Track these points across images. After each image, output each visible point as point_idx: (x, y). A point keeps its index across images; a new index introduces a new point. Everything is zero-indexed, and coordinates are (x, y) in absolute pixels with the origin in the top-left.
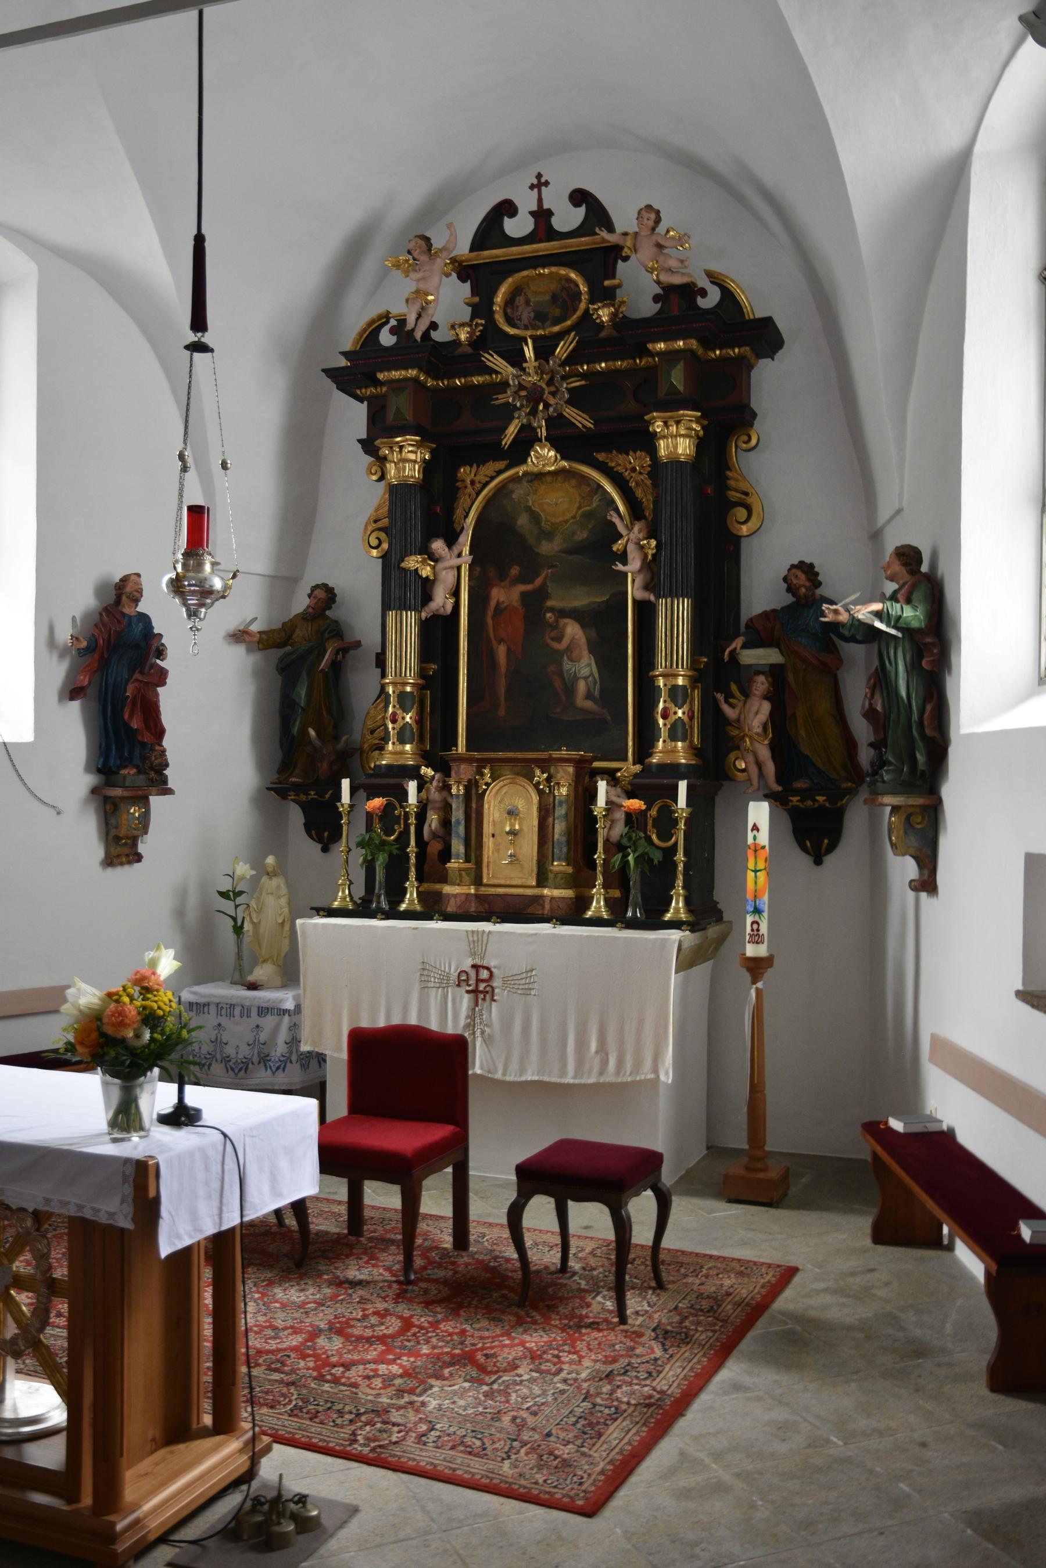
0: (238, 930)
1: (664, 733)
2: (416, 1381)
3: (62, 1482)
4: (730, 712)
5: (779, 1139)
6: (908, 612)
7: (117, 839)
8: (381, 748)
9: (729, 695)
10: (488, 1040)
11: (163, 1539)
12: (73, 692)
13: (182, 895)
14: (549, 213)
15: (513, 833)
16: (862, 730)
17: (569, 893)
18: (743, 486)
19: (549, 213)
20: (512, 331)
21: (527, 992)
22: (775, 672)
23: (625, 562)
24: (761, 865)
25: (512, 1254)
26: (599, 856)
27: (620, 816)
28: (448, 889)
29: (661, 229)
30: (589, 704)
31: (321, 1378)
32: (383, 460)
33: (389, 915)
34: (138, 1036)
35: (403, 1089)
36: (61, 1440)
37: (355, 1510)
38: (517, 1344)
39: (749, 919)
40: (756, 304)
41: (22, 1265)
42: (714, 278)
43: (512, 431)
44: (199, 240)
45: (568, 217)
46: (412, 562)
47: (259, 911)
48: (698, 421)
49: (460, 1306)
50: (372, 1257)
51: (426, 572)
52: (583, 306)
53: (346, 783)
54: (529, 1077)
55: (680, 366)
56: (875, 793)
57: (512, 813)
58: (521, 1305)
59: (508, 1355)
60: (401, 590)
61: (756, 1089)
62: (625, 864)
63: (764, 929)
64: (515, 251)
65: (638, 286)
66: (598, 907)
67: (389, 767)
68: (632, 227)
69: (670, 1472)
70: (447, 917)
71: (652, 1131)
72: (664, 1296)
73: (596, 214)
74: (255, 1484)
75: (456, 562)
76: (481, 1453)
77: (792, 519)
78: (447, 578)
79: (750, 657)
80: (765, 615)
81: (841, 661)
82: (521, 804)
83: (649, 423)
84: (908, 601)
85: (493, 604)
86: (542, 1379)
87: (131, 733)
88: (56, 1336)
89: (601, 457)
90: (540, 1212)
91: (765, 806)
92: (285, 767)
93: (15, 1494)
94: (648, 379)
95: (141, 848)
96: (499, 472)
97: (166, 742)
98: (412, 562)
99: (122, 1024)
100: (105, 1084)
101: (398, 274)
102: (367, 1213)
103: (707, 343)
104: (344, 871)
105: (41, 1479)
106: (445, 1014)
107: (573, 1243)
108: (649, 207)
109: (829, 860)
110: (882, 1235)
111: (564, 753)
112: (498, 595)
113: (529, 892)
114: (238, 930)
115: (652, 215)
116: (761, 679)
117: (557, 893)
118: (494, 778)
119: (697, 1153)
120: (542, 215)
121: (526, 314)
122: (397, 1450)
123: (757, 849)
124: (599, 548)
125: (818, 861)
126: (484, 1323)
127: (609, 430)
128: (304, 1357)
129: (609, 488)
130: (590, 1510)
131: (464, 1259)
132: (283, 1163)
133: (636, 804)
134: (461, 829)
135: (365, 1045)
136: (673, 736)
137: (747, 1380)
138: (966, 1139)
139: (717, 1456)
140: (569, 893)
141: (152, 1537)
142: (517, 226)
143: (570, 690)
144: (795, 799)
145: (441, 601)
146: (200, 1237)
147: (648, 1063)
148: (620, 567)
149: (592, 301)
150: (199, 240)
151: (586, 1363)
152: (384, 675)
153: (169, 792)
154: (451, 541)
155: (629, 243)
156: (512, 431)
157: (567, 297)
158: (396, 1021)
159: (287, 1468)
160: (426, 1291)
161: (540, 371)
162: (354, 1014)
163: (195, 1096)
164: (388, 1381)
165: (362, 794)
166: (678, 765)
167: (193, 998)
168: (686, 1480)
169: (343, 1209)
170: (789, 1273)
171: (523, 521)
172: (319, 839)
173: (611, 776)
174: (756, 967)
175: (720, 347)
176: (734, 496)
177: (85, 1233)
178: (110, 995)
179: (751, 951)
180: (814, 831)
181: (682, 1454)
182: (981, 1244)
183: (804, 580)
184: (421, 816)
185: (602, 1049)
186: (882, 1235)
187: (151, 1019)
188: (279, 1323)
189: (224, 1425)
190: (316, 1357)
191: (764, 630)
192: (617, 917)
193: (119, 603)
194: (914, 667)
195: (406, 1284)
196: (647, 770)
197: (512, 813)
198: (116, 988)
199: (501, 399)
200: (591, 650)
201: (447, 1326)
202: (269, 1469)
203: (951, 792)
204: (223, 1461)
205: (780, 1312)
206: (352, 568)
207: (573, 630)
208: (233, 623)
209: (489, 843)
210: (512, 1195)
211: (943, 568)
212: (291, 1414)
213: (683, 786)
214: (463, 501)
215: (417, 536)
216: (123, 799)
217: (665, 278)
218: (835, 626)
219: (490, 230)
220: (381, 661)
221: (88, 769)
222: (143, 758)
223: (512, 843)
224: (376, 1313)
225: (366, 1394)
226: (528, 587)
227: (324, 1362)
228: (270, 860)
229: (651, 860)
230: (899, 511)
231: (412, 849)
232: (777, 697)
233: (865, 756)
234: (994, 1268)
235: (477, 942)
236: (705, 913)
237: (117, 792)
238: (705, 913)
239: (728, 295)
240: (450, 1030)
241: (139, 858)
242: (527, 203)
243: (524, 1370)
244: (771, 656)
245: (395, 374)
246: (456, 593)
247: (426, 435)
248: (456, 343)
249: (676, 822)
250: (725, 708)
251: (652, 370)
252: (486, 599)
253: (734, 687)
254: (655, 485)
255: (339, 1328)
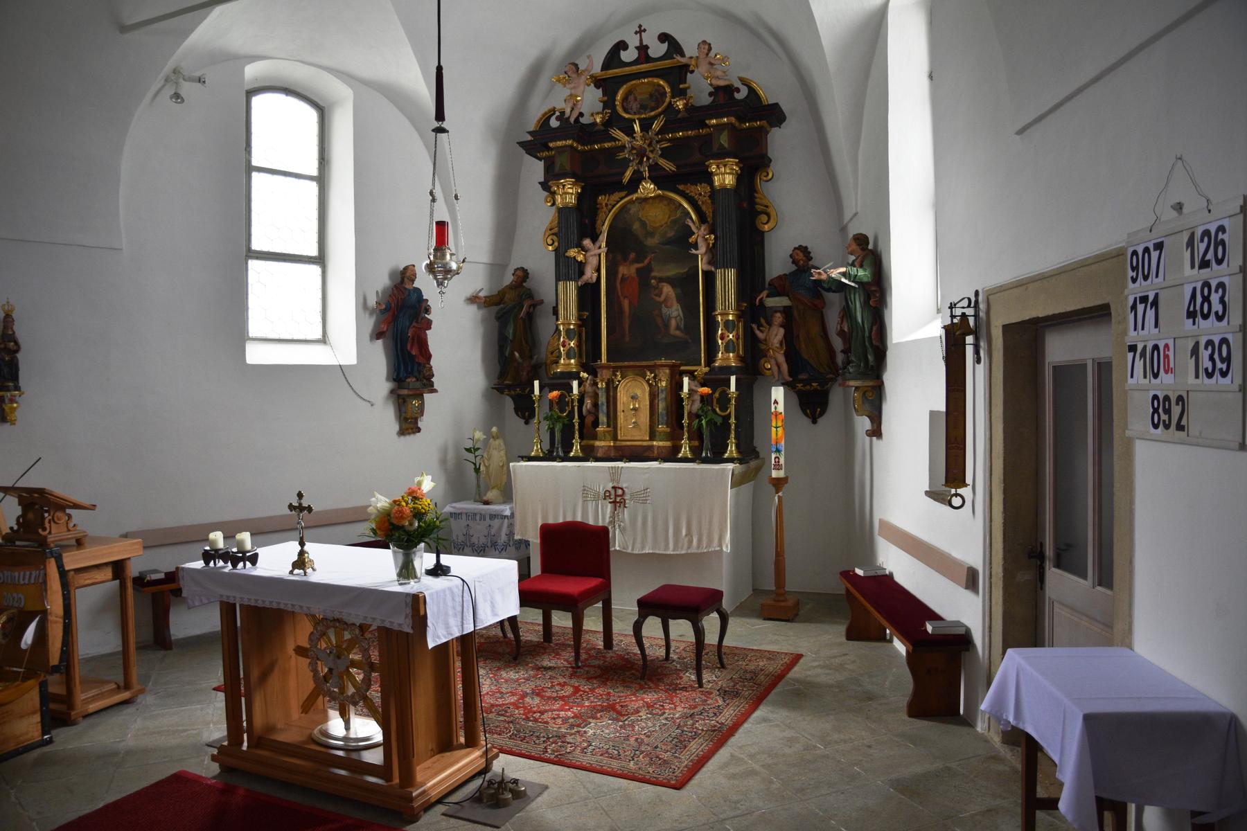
0: (477, 470)
1: (722, 348)
2: (582, 720)
3: (383, 771)
4: (761, 335)
5: (793, 584)
6: (861, 273)
7: (406, 419)
8: (557, 362)
9: (759, 326)
10: (623, 530)
11: (439, 801)
12: (378, 335)
13: (444, 451)
14: (647, 47)
15: (635, 409)
16: (838, 343)
17: (668, 444)
18: (765, 202)
19: (647, 47)
20: (626, 116)
21: (644, 502)
22: (786, 311)
23: (697, 249)
24: (780, 424)
25: (637, 650)
26: (685, 421)
27: (697, 398)
28: (597, 443)
29: (712, 54)
30: (678, 333)
31: (527, 719)
32: (553, 194)
33: (563, 460)
34: (411, 524)
35: (570, 560)
36: (381, 750)
37: (547, 787)
38: (638, 700)
39: (773, 456)
40: (768, 97)
41: (355, 656)
42: (744, 82)
43: (628, 174)
44: (439, 70)
45: (657, 49)
46: (572, 253)
47: (489, 459)
48: (737, 164)
49: (608, 679)
50: (558, 654)
51: (580, 258)
52: (668, 100)
53: (536, 383)
54: (647, 551)
55: (725, 133)
56: (845, 380)
57: (634, 398)
58: (642, 678)
59: (633, 706)
60: (567, 269)
61: (779, 555)
62: (700, 425)
63: (782, 461)
64: (627, 70)
65: (700, 87)
66: (685, 451)
67: (562, 373)
68: (695, 53)
69: (724, 766)
70: (597, 460)
71: (720, 579)
72: (725, 672)
73: (674, 46)
74: (488, 776)
75: (598, 251)
76: (618, 757)
77: (794, 220)
78: (593, 261)
79: (771, 302)
80: (780, 277)
81: (824, 303)
82: (639, 393)
83: (708, 166)
84: (861, 266)
85: (620, 276)
86: (652, 718)
87: (412, 357)
88: (375, 693)
89: (681, 187)
90: (653, 627)
91: (781, 389)
92: (502, 375)
93: (358, 777)
94: (707, 141)
95: (420, 424)
96: (622, 198)
97: (432, 363)
98: (572, 253)
99: (402, 518)
100: (394, 552)
101: (560, 86)
102: (554, 630)
103: (741, 119)
104: (537, 435)
105: (371, 769)
106: (597, 515)
107: (673, 645)
108: (704, 42)
109: (820, 421)
110: (852, 635)
111: (663, 361)
112: (623, 270)
113: (645, 444)
114: (477, 470)
115: (706, 46)
116: (778, 315)
117: (661, 444)
118: (623, 377)
119: (747, 593)
120: (642, 49)
121: (635, 106)
122: (570, 757)
123: (777, 414)
124: (682, 241)
125: (814, 422)
126: (621, 689)
127: (685, 172)
128: (518, 708)
129: (686, 205)
130: (679, 786)
131: (610, 654)
132: (498, 597)
133: (706, 390)
134: (605, 408)
135: (550, 533)
136: (727, 350)
137: (771, 716)
138: (900, 579)
139: (752, 756)
140: (668, 444)
141: (433, 800)
142: (628, 56)
143: (667, 326)
144: (800, 385)
145: (590, 275)
146: (450, 638)
147: (716, 541)
148: (694, 251)
149: (673, 97)
150: (439, 70)
151: (679, 709)
152: (557, 319)
153: (435, 391)
154: (594, 239)
155: (693, 62)
156: (628, 174)
157: (658, 95)
158: (569, 519)
159: (507, 765)
160: (588, 672)
161: (644, 138)
162: (545, 516)
163: (446, 559)
164: (565, 720)
165: (547, 389)
166: (730, 367)
167: (452, 510)
168: (733, 770)
169: (541, 628)
170: (798, 657)
171: (636, 226)
172: (523, 417)
173: (691, 375)
174: (778, 484)
175: (749, 122)
176: (759, 208)
177: (387, 635)
178: (395, 502)
179: (774, 474)
180: (811, 403)
181: (732, 756)
182: (906, 637)
183: (802, 258)
184: (581, 401)
185: (689, 534)
186: (852, 635)
187: (418, 515)
188: (504, 690)
189: (471, 743)
190: (525, 708)
191: (778, 288)
192: (697, 457)
193: (404, 277)
194: (866, 304)
195: (577, 669)
196: (712, 370)
197: (634, 398)
198: (398, 498)
199: (621, 156)
200: (679, 301)
201: (600, 691)
202: (497, 766)
203: (889, 378)
204: (471, 761)
205: (797, 680)
206: (537, 256)
207: (667, 289)
208: (469, 292)
209: (621, 416)
210: (636, 617)
211: (881, 246)
212: (510, 738)
213: (733, 379)
214: (601, 215)
215: (575, 237)
216: (408, 396)
217: (715, 82)
218: (818, 283)
219: (613, 58)
220: (555, 312)
221: (388, 379)
222: (419, 372)
223: (635, 415)
224: (559, 684)
225: (553, 727)
226: (640, 265)
227: (529, 711)
228: (494, 429)
229: (715, 423)
230: (856, 214)
231: (576, 420)
232: (788, 326)
233: (840, 358)
234: (911, 648)
235: (615, 473)
236: (748, 453)
237: (405, 392)
238: (748, 453)
239: (752, 91)
240: (600, 524)
241: (419, 430)
242: (633, 42)
243: (643, 714)
244: (783, 301)
245: (559, 143)
246: (598, 270)
247: (578, 179)
248: (595, 124)
249: (730, 400)
250: (757, 332)
251: (710, 135)
252: (616, 273)
253: (762, 321)
254: (713, 203)
255: (538, 693)
